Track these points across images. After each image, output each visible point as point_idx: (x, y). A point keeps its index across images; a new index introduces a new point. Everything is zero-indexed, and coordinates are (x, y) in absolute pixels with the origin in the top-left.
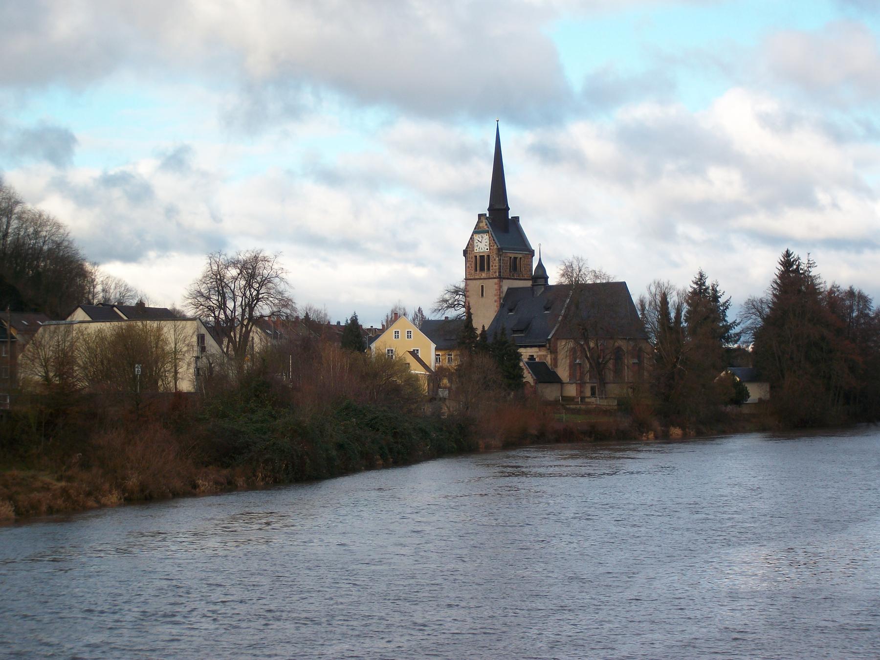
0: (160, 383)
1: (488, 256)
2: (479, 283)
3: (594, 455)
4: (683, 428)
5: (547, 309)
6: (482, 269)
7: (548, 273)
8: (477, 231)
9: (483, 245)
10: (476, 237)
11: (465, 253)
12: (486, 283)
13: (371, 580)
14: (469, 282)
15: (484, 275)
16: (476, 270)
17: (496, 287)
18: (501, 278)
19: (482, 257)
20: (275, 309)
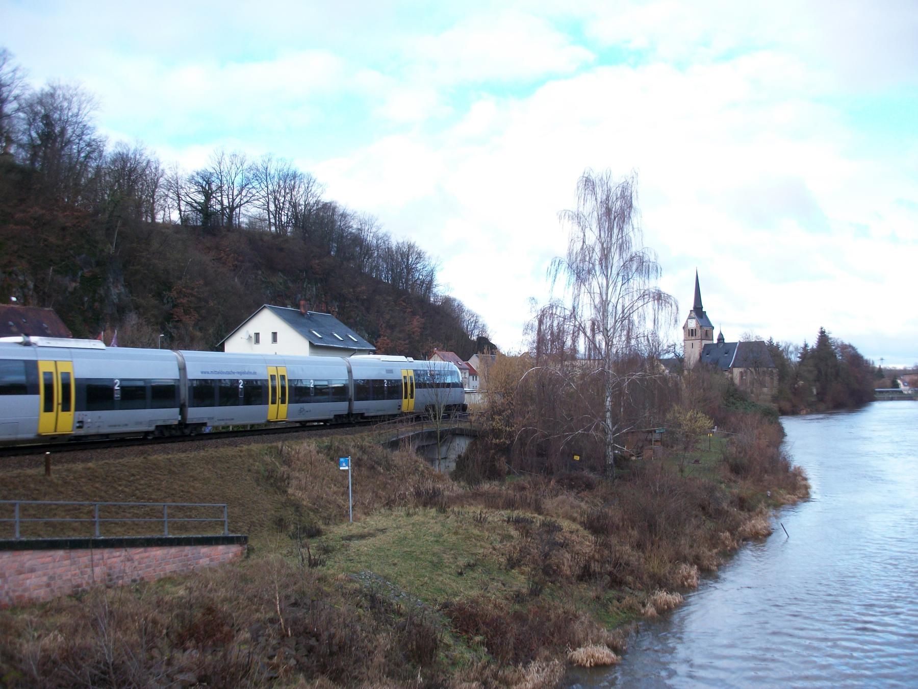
8: (690, 317)
9: (693, 324)
10: (690, 321)
18: (702, 339)
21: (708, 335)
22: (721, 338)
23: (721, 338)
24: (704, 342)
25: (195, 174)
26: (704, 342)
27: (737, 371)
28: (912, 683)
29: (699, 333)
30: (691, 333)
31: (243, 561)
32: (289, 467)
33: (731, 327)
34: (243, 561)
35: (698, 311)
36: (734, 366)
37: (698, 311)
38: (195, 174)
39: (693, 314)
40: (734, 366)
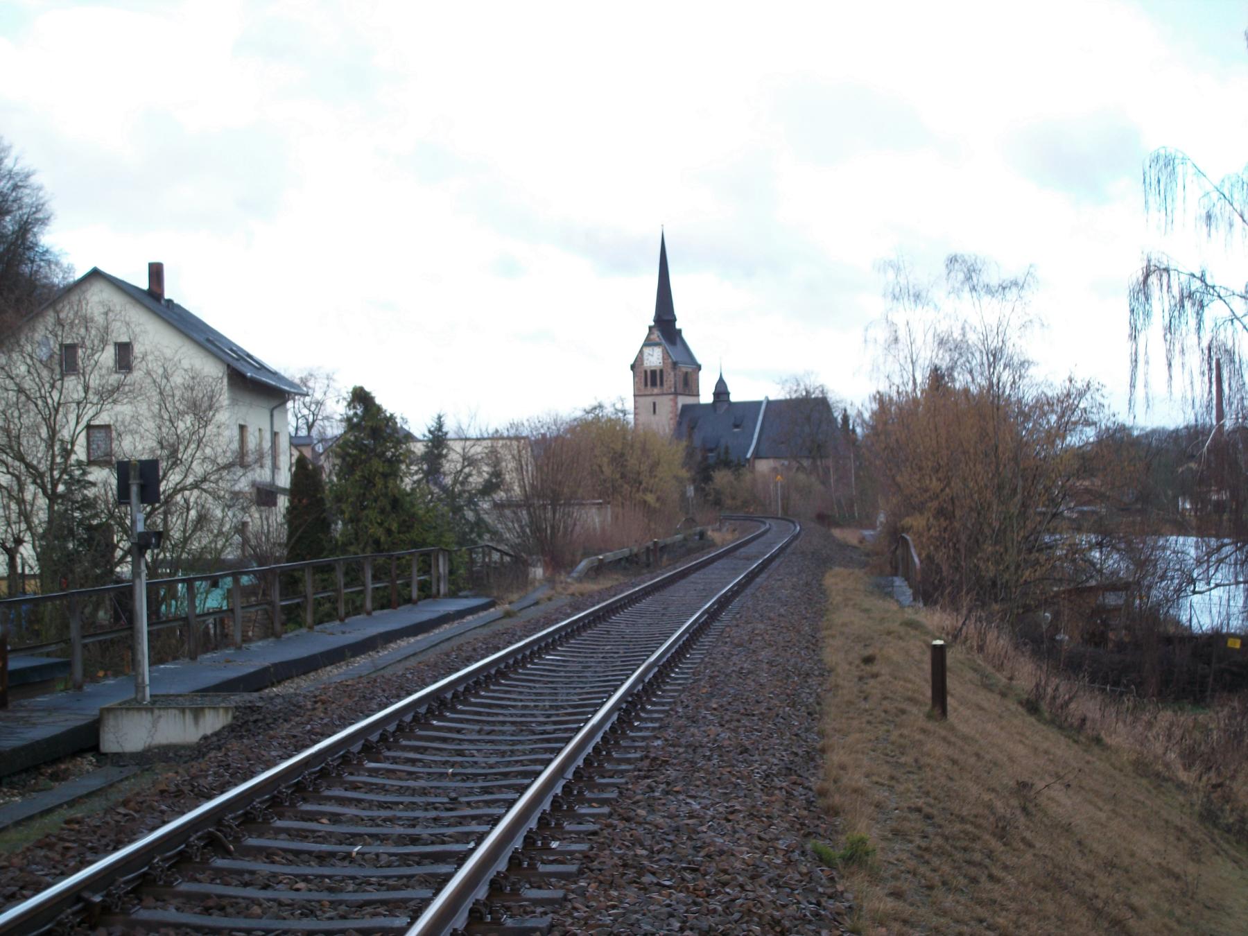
0: (163, 607)
1: (661, 371)
2: (650, 400)
3: (50, 720)
4: (106, 670)
5: (737, 426)
6: (654, 384)
7: (730, 389)
8: (648, 343)
9: (655, 358)
10: (647, 351)
11: (633, 367)
12: (659, 400)
13: (944, 883)
14: (639, 399)
15: (656, 391)
16: (646, 385)
17: (671, 403)
18: (676, 394)
19: (653, 372)
20: (982, 293)
21: (689, 383)
22: (721, 391)
23: (721, 391)
24: (683, 400)
25: (1180, 156)
26: (683, 400)
27: (763, 466)
28: (1096, 788)
29: (670, 378)
30: (647, 379)
31: (41, 361)
32: (905, 901)
33: (746, 362)
34: (41, 361)
35: (665, 325)
36: (757, 455)
37: (665, 325)
38: (1180, 156)
39: (656, 335)
40: (757, 455)
